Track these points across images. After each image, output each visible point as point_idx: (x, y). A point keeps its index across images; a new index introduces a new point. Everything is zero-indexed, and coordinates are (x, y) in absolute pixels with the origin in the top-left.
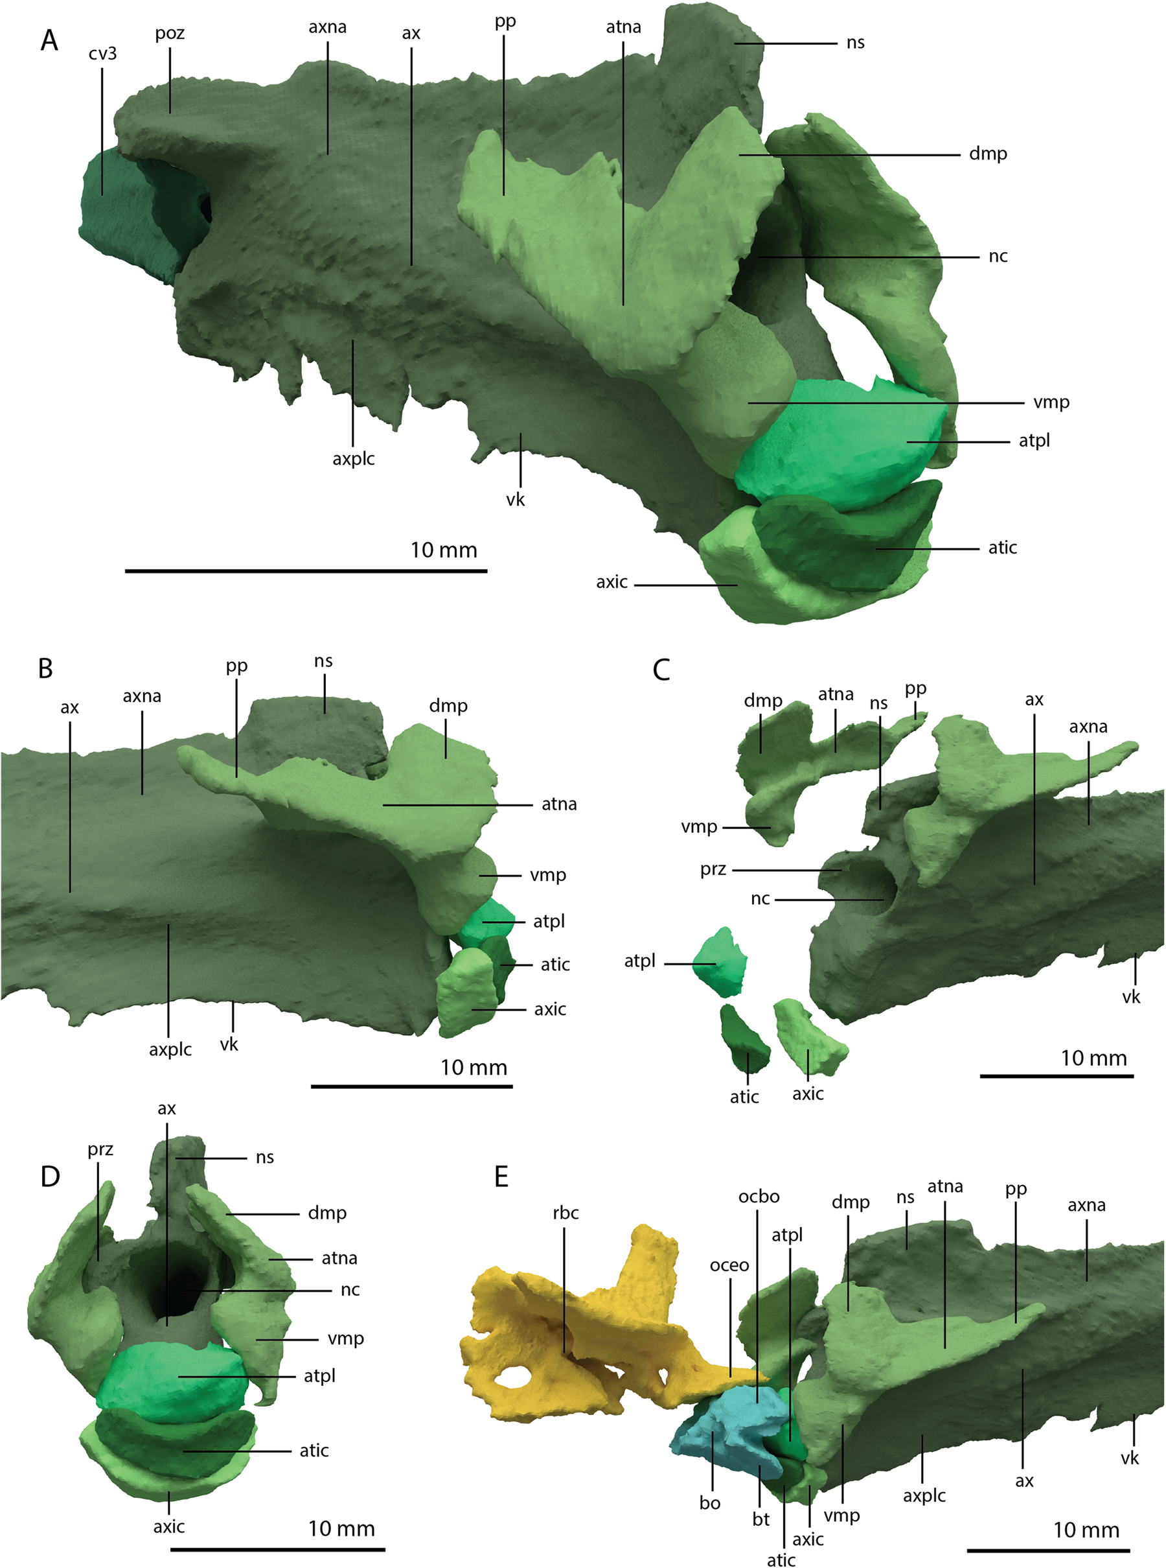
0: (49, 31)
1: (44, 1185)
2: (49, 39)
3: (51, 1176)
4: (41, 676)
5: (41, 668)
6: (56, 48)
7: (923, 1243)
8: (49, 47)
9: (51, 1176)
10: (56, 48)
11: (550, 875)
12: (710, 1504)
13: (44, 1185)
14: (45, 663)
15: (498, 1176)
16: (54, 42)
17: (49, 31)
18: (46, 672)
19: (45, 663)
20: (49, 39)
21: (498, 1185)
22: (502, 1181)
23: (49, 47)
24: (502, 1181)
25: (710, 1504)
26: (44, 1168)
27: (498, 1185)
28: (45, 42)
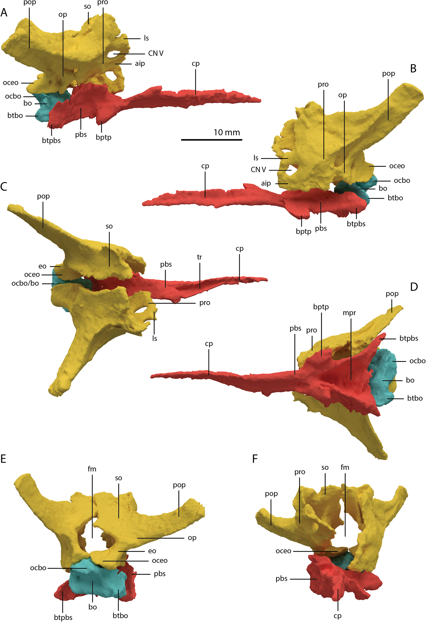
0: (4, 9)
1: (412, 290)
2: (4, 12)
3: (414, 286)
4: (412, 72)
5: (412, 68)
6: (7, 16)
7: (64, 586)
8: (4, 15)
9: (414, 286)
10: (7, 16)
11: (347, 313)
12: (93, 608)
13: (412, 290)
14: (413, 66)
15: (2, 458)
16: (6, 13)
17: (4, 9)
18: (413, 70)
19: (413, 66)
20: (4, 12)
21: (2, 462)
22: (3, 460)
23: (4, 15)
24: (3, 460)
25: (93, 608)
26: (412, 283)
27: (2, 462)
28: (2, 13)
